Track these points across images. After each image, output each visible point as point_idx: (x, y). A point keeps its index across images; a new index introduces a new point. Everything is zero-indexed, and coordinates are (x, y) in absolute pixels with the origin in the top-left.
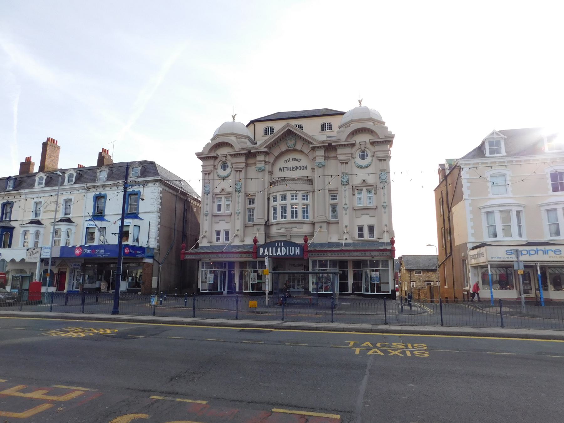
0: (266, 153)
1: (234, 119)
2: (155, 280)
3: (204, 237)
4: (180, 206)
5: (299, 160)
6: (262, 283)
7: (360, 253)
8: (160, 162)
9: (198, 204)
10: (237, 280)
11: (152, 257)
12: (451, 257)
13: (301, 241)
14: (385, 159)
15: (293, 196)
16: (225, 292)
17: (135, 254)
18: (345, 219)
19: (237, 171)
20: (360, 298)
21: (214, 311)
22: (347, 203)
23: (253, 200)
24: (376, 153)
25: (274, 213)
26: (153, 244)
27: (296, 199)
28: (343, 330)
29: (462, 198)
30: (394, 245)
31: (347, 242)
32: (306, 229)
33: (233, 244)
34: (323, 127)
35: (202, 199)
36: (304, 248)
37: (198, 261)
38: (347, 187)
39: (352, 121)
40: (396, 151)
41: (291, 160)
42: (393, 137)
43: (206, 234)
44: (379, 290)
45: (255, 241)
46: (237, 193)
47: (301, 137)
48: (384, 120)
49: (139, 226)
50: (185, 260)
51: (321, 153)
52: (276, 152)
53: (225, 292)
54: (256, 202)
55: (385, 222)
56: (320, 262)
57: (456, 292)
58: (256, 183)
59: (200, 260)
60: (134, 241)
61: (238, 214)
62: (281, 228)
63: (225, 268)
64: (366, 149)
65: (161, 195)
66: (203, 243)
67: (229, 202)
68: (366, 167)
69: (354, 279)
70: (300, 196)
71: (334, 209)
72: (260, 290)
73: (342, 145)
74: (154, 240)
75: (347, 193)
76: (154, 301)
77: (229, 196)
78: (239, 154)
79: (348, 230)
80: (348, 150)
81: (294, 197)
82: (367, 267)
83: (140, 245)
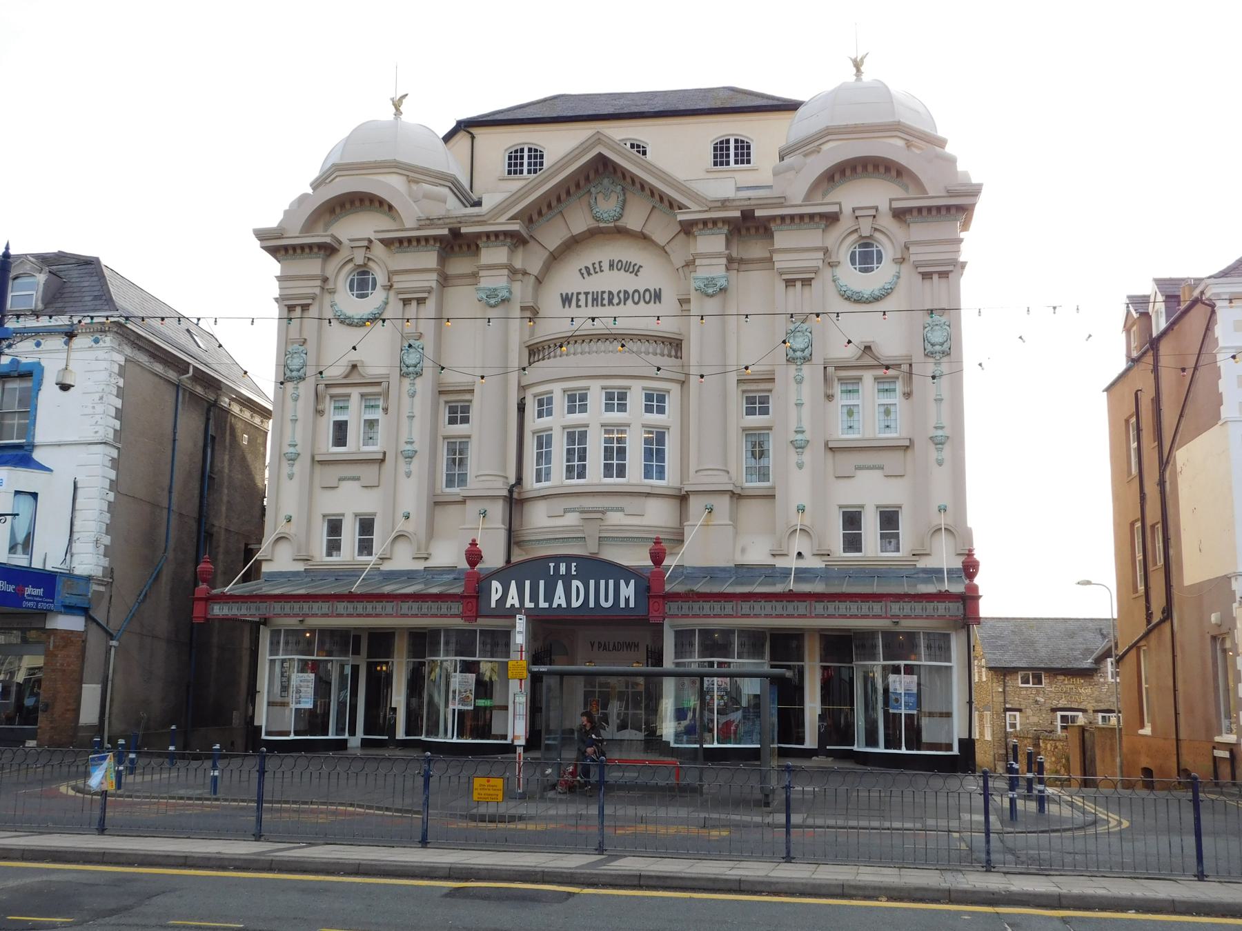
0: (516, 240)
1: (398, 112)
2: (90, 694)
3: (280, 539)
4: (190, 425)
5: (634, 270)
6: (491, 708)
7: (843, 607)
8: (117, 260)
9: (257, 420)
10: (399, 698)
11: (84, 611)
12: (1166, 627)
13: (639, 559)
14: (945, 271)
15: (610, 397)
16: (354, 742)
17: (18, 598)
18: (797, 482)
19: (406, 302)
20: (848, 765)
21: (327, 812)
22: (806, 425)
23: (466, 409)
24: (912, 250)
25: (539, 456)
26: (88, 562)
27: (622, 408)
28: (843, 891)
29: (1217, 416)
30: (977, 581)
31: (803, 564)
32: (657, 515)
33: (386, 567)
34: (721, 153)
35: (274, 404)
36: (651, 586)
37: (255, 627)
38: (806, 369)
39: (828, 133)
41: (606, 266)
42: (974, 192)
43: (291, 529)
44: (915, 739)
45: (474, 556)
46: (406, 381)
47: (643, 186)
48: (941, 133)
49: (35, 495)
50: (208, 622)
51: (713, 243)
52: (553, 236)
53: (354, 742)
54: (474, 414)
55: (940, 494)
56: (706, 633)
57: (1183, 751)
58: (476, 344)
59: (265, 622)
60: (12, 549)
61: (410, 457)
62: (566, 511)
63: (356, 652)
64: (877, 235)
65: (121, 383)
66: (278, 559)
67: (377, 415)
69: (824, 700)
70: (636, 399)
71: (758, 450)
72: (485, 731)
73: (792, 217)
74: (90, 547)
75: (806, 388)
76: (100, 777)
77: (375, 391)
78: (418, 239)
79: (807, 522)
80: (811, 237)
81: (617, 400)
82: (873, 657)
83: (37, 564)
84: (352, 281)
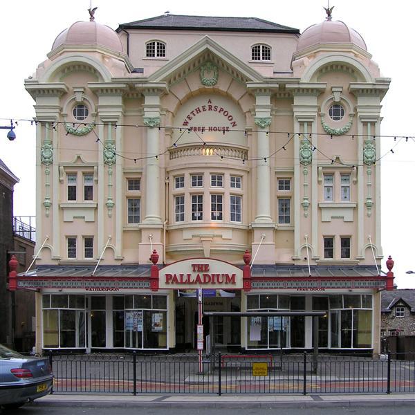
0: (161, 93)
1: (92, 18)
16: (88, 351)
30: (392, 271)
40: (393, 113)
42: (387, 82)
48: (370, 51)
51: (264, 101)
53: (88, 351)
56: (263, 296)
68: (83, 134)
78: (111, 89)
80: (313, 101)
81: (217, 179)
84: (75, 110)
